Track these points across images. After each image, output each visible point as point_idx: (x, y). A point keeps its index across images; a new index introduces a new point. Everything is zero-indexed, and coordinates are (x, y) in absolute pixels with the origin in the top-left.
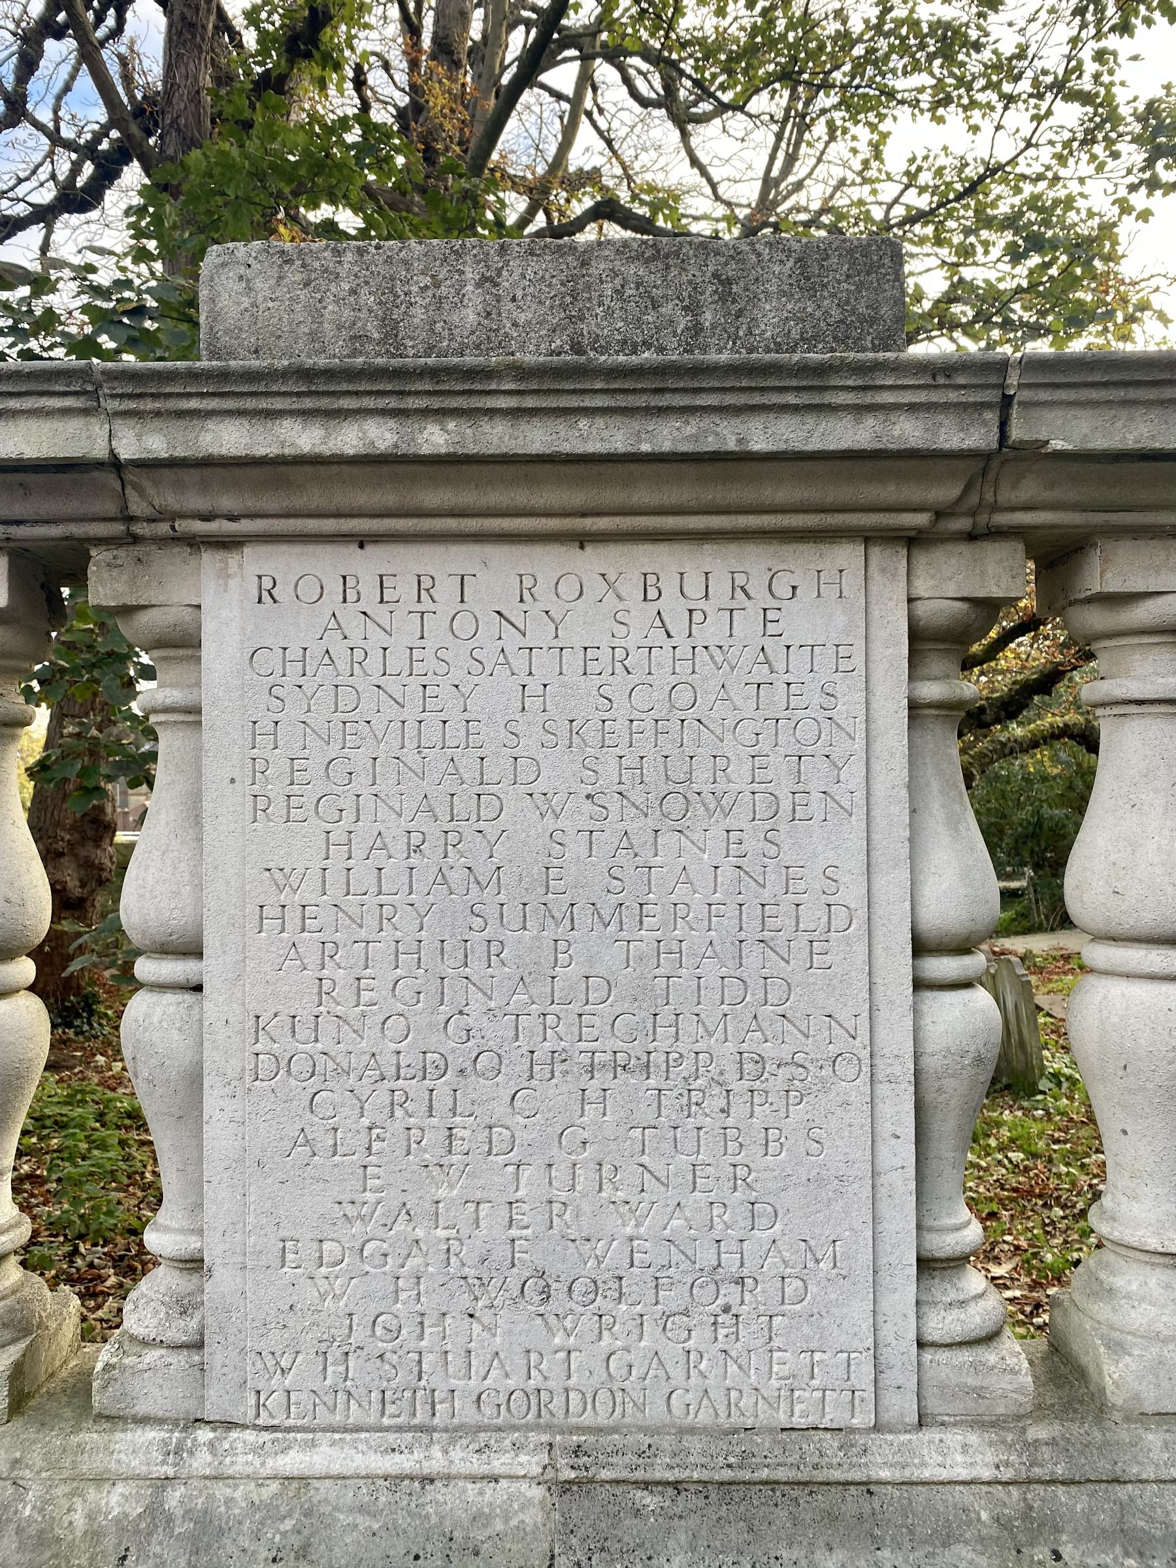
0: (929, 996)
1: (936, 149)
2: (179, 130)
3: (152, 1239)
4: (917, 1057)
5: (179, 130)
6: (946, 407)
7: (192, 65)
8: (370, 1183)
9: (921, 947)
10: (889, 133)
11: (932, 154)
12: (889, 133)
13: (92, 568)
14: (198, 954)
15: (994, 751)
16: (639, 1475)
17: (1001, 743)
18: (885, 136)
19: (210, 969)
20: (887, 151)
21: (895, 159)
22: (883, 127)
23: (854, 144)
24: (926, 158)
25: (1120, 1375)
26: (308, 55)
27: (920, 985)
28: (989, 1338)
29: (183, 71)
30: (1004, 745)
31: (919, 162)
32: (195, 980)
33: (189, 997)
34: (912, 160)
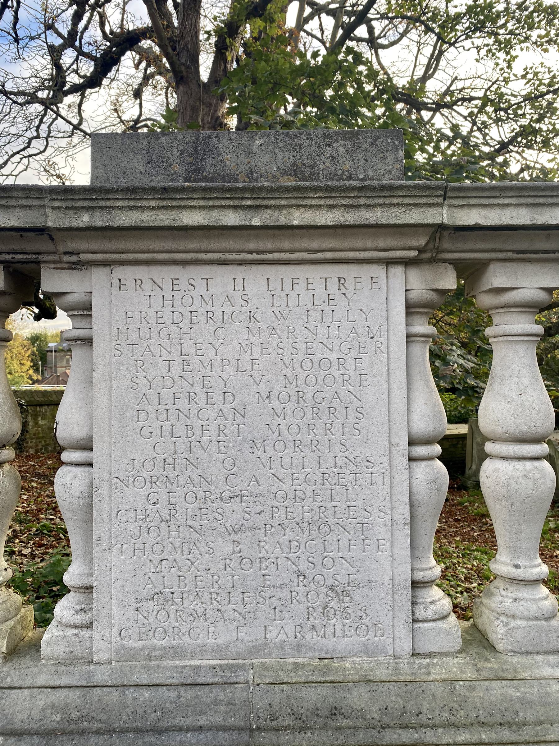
0: (414, 464)
1: (537, 64)
2: (188, 51)
3: (66, 579)
4: (411, 493)
5: (188, 51)
6: (229, 207)
7: (194, 20)
8: (381, 547)
9: (412, 443)
10: (516, 57)
11: (535, 66)
12: (516, 57)
13: (42, 270)
14: (91, 449)
15: (551, 347)
16: (394, 678)
17: (553, 343)
18: (514, 58)
19: (96, 456)
20: (514, 65)
21: (518, 68)
22: (513, 53)
23: (498, 61)
24: (531, 68)
25: (498, 632)
26: (260, 16)
27: (411, 459)
28: (445, 617)
29: (190, 22)
30: (554, 344)
31: (528, 70)
32: (89, 461)
33: (87, 469)
34: (526, 69)
